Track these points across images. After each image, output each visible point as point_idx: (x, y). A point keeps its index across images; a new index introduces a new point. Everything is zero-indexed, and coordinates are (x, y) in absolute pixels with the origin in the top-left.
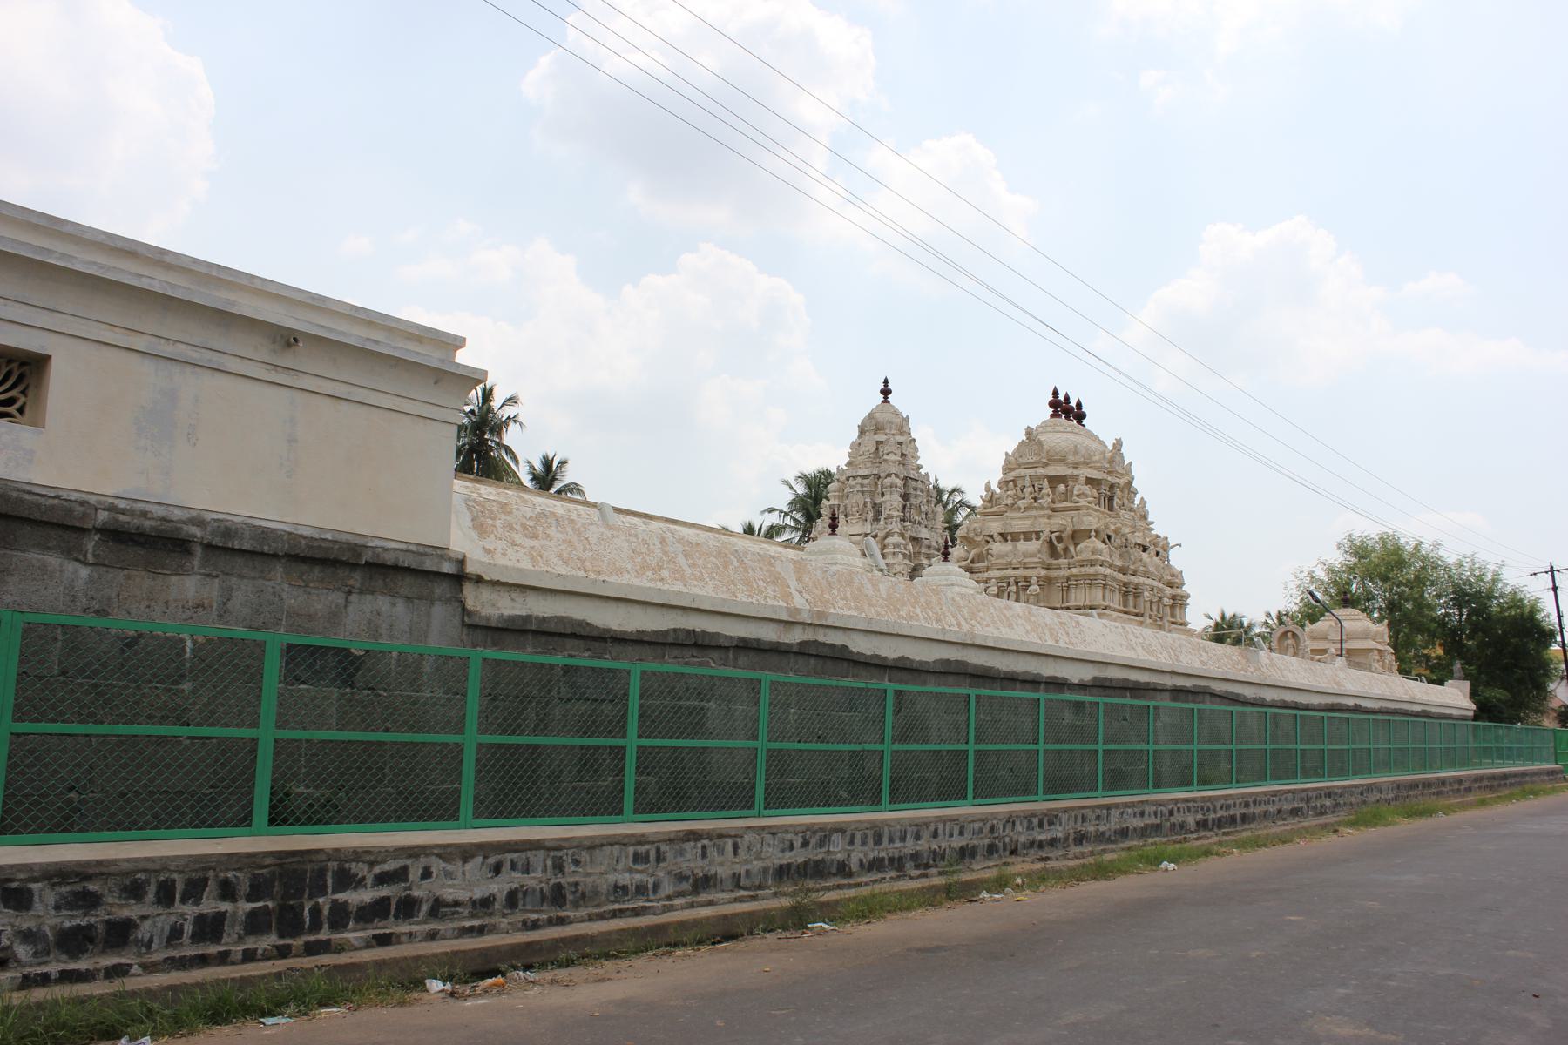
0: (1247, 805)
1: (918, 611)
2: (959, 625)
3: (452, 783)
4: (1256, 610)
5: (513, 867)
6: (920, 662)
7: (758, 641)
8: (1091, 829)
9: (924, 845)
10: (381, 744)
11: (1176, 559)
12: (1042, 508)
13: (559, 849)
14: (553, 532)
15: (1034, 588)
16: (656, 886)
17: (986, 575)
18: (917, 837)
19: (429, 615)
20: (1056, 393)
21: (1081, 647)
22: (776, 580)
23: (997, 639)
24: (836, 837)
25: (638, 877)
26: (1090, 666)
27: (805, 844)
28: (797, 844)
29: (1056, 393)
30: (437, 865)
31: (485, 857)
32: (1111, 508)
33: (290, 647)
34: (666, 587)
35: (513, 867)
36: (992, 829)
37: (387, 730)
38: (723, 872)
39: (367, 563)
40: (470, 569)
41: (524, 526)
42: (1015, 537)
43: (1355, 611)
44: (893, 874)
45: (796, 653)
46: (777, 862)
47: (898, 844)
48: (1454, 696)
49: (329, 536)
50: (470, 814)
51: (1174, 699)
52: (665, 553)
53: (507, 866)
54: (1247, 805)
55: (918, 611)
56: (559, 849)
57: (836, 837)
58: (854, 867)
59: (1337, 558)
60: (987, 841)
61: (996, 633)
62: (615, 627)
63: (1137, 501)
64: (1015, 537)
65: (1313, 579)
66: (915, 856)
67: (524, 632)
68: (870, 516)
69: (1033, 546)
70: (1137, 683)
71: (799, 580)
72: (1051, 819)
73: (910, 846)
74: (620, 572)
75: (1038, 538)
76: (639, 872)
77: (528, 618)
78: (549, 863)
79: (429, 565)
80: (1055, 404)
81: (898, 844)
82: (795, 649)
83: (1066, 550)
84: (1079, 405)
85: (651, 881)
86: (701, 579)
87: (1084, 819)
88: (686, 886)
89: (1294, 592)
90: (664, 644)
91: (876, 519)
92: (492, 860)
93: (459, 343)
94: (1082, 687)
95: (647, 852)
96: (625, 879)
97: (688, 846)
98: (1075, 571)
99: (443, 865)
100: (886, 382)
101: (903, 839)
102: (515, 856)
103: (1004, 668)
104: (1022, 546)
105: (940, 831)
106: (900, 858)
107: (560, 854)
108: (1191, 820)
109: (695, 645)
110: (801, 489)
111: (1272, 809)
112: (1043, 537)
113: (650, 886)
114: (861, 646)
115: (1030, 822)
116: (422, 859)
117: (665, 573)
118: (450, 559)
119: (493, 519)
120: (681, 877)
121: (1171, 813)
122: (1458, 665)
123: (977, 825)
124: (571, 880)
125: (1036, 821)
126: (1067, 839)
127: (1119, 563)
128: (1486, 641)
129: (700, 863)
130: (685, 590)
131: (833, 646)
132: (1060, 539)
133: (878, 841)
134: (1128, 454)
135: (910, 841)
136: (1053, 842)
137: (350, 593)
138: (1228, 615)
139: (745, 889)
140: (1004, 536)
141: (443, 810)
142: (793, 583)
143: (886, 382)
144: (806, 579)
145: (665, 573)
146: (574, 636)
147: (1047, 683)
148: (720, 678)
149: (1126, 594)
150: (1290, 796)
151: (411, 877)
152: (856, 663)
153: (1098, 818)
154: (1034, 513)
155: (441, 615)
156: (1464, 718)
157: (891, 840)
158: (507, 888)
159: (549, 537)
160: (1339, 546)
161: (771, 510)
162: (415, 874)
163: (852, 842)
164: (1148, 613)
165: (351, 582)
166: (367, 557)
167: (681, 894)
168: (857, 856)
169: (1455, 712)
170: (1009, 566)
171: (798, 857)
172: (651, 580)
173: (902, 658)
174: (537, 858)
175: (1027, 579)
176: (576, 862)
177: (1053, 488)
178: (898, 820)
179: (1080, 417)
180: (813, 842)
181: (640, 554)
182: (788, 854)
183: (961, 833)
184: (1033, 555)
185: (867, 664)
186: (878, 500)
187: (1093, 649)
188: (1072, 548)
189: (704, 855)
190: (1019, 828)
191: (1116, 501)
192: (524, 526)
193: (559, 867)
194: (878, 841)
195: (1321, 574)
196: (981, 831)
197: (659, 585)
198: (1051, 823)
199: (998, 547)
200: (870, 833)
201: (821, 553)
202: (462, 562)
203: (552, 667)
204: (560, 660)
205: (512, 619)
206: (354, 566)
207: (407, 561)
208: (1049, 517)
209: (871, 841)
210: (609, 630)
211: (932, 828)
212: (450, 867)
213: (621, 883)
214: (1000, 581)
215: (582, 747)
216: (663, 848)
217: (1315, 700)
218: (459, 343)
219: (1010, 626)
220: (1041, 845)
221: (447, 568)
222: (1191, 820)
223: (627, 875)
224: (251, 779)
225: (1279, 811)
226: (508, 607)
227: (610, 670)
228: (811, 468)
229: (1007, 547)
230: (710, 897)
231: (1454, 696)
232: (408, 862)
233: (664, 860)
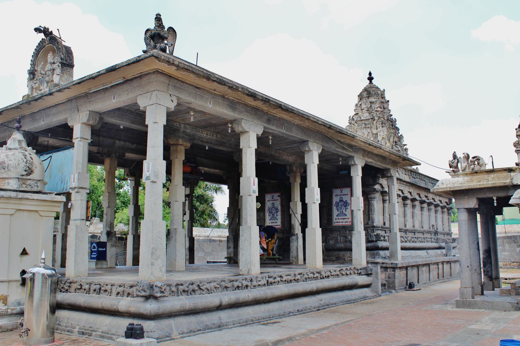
100: (370, 74)
143: (370, 74)
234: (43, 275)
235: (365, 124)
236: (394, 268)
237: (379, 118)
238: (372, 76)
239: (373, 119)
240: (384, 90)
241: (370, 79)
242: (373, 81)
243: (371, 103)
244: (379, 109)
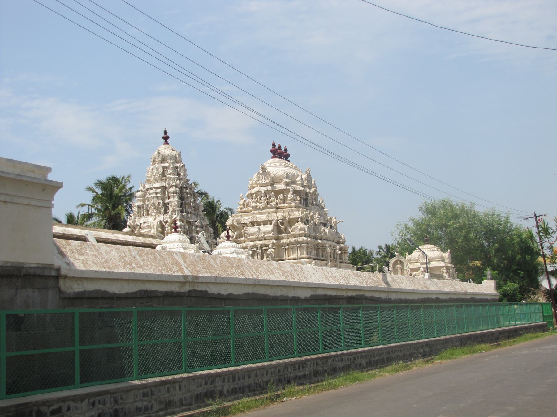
0: (389, 353)
1: (234, 271)
2: (252, 275)
4: (372, 244)
5: (99, 403)
6: (237, 295)
7: (172, 292)
8: (321, 369)
9: (251, 381)
10: (33, 355)
12: (272, 208)
13: (115, 393)
14: (88, 251)
15: (271, 250)
16: (152, 407)
17: (244, 245)
18: (249, 377)
21: (305, 281)
22: (176, 263)
23: (269, 281)
24: (218, 379)
25: (145, 403)
26: (309, 290)
27: (206, 383)
28: (203, 383)
30: (72, 404)
31: (89, 399)
32: (307, 205)
33: (7, 315)
34: (136, 272)
35: (99, 403)
36: (279, 371)
37: (35, 349)
38: (176, 399)
39: (24, 275)
40: (63, 272)
41: (76, 249)
42: (258, 224)
43: (432, 246)
44: (242, 395)
45: (187, 296)
46: (196, 392)
47: (242, 381)
48: (488, 287)
49: (9, 265)
50: (79, 382)
51: (348, 303)
52: (131, 255)
53: (97, 403)
54: (389, 353)
55: (234, 271)
56: (115, 393)
57: (218, 379)
58: (225, 392)
59: (419, 216)
60: (277, 377)
61: (268, 278)
62: (117, 292)
64: (258, 224)
65: (406, 227)
66: (249, 386)
67: (82, 298)
68: (162, 210)
69: (269, 228)
70: (331, 296)
71: (185, 262)
72: (303, 364)
73: (246, 382)
74: (117, 266)
75: (271, 224)
76: (145, 401)
77: (84, 292)
78: (112, 400)
79: (47, 273)
81: (242, 381)
82: (186, 295)
83: (286, 229)
85: (150, 404)
86: (147, 266)
87: (317, 365)
88: (163, 406)
89: (397, 237)
90: (136, 298)
91: (166, 212)
92: (91, 401)
93: (49, 170)
94: (307, 300)
95: (148, 392)
96: (140, 404)
97: (162, 388)
98: (292, 240)
99: (74, 404)
100: (165, 132)
101: (244, 379)
102: (99, 398)
103: (272, 295)
104: (263, 228)
105: (258, 374)
106: (243, 387)
107: (116, 395)
108: (364, 362)
109: (148, 297)
110: (99, 191)
111: (401, 354)
112: (274, 222)
113: (150, 407)
114: (213, 290)
115: (294, 367)
116: (67, 402)
117: (134, 265)
118: (54, 269)
119: (65, 248)
120: (161, 402)
121: (355, 359)
122: (488, 272)
123: (273, 370)
124: (121, 407)
125: (297, 366)
126: (310, 374)
127: (313, 234)
128: (503, 256)
129: (167, 395)
130: (143, 272)
131: (201, 291)
132: (282, 224)
133: (234, 380)
135: (247, 379)
136: (304, 376)
137: (17, 289)
138: (357, 248)
139: (185, 405)
141: (66, 381)
142: (182, 263)
143: (165, 132)
144: (187, 260)
145: (134, 265)
146: (102, 298)
147: (291, 300)
148: (158, 311)
149: (318, 250)
150: (408, 347)
151: (63, 411)
152: (211, 298)
153: (323, 363)
154: (268, 210)
155: (51, 294)
156: (494, 300)
157: (239, 379)
158: (97, 412)
159: (87, 254)
160: (420, 209)
161: (83, 205)
162: (64, 409)
163: (224, 382)
164: (329, 259)
165: (17, 284)
166: (24, 272)
167: (161, 410)
168: (227, 387)
169: (489, 298)
170: (258, 239)
171: (201, 390)
172: (130, 269)
173: (230, 294)
174: (108, 398)
175: (267, 246)
176: (122, 399)
178: (241, 370)
180: (209, 382)
181: (122, 257)
182: (200, 389)
183: (267, 374)
184: (269, 233)
185: (215, 298)
186: (167, 201)
187: (310, 281)
189: (168, 391)
190: (290, 370)
191: (309, 201)
192: (76, 249)
193: (116, 401)
194: (234, 380)
195: (411, 225)
196: (274, 372)
197: (133, 271)
198: (303, 367)
199: (253, 230)
200: (231, 376)
201: (171, 242)
202: (58, 270)
203: (94, 313)
204: (97, 310)
205: (79, 293)
206: (18, 277)
207: (38, 272)
208: (276, 213)
209: (231, 380)
210: (115, 294)
211: (255, 372)
212: (77, 405)
213: (139, 406)
214: (252, 247)
215: (108, 349)
216: (154, 389)
217: (416, 297)
218: (49, 170)
219: (273, 273)
220: (300, 378)
221: (53, 273)
222: (364, 362)
223: (141, 403)
224: (74, 360)
225: (404, 355)
226: (77, 288)
227: (116, 312)
228: (103, 178)
229: (254, 229)
230: (173, 410)
231: (488, 287)
232: (62, 404)
233: (154, 395)
238: (168, 134)
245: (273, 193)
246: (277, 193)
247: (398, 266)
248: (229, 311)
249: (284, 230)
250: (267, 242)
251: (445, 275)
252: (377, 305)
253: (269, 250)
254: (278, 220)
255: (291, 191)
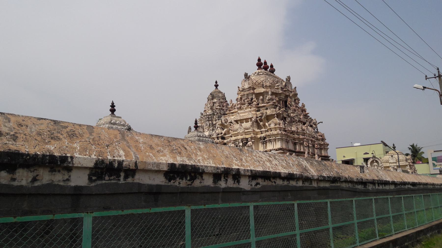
3: (303, 237)
11: (321, 129)
19: (76, 157)
20: (259, 60)
29: (259, 60)
63: (300, 105)
69: (249, 124)
80: (259, 65)
83: (264, 125)
84: (272, 66)
98: (268, 133)
100: (216, 82)
104: (245, 125)
134: (294, 83)
140: (237, 121)
143: (216, 82)
175: (247, 139)
177: (258, 99)
179: (273, 71)
188: (267, 124)
199: (237, 126)
234: (394, 222)
235: (208, 118)
236: (426, 209)
237: (217, 114)
238: (218, 83)
239: (214, 114)
240: (288, 79)
241: (216, 86)
242: (115, 113)
243: (214, 103)
244: (218, 107)
245: (254, 95)
246: (258, 95)
247: (375, 164)
248: (249, 207)
249: (262, 126)
250: (247, 136)
251: (409, 170)
252: (371, 198)
253: (249, 143)
254: (257, 117)
255: (270, 93)
